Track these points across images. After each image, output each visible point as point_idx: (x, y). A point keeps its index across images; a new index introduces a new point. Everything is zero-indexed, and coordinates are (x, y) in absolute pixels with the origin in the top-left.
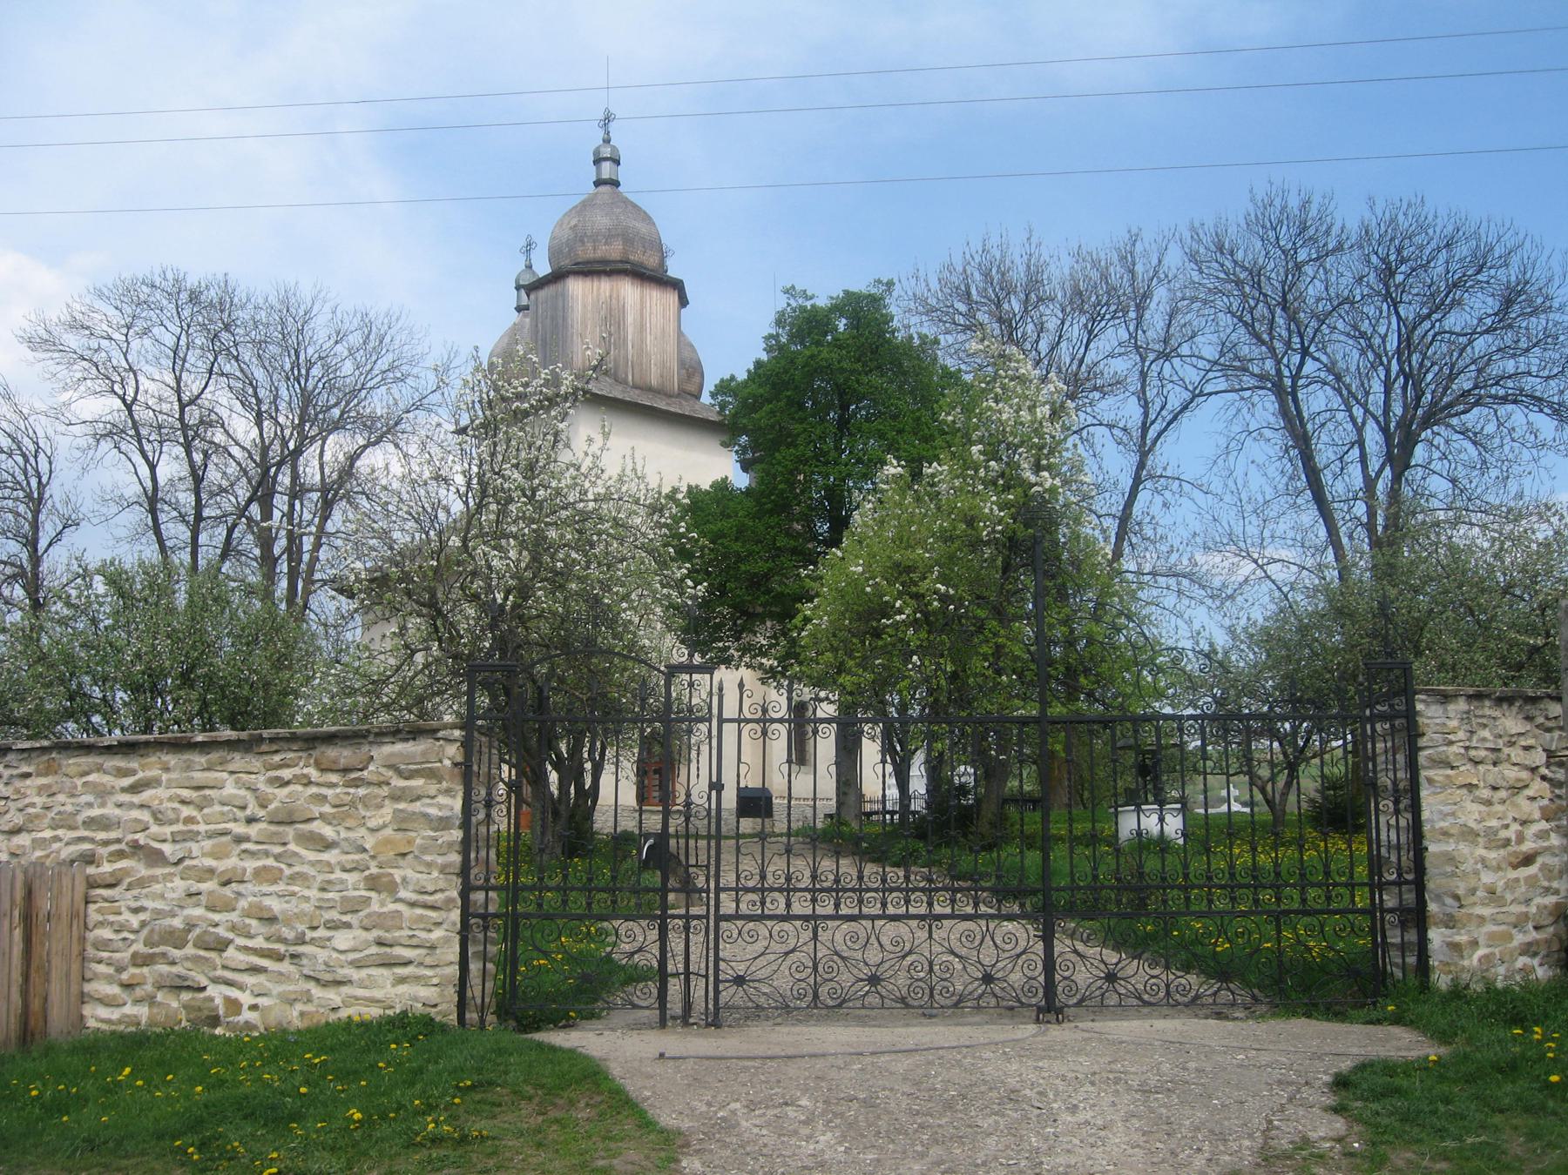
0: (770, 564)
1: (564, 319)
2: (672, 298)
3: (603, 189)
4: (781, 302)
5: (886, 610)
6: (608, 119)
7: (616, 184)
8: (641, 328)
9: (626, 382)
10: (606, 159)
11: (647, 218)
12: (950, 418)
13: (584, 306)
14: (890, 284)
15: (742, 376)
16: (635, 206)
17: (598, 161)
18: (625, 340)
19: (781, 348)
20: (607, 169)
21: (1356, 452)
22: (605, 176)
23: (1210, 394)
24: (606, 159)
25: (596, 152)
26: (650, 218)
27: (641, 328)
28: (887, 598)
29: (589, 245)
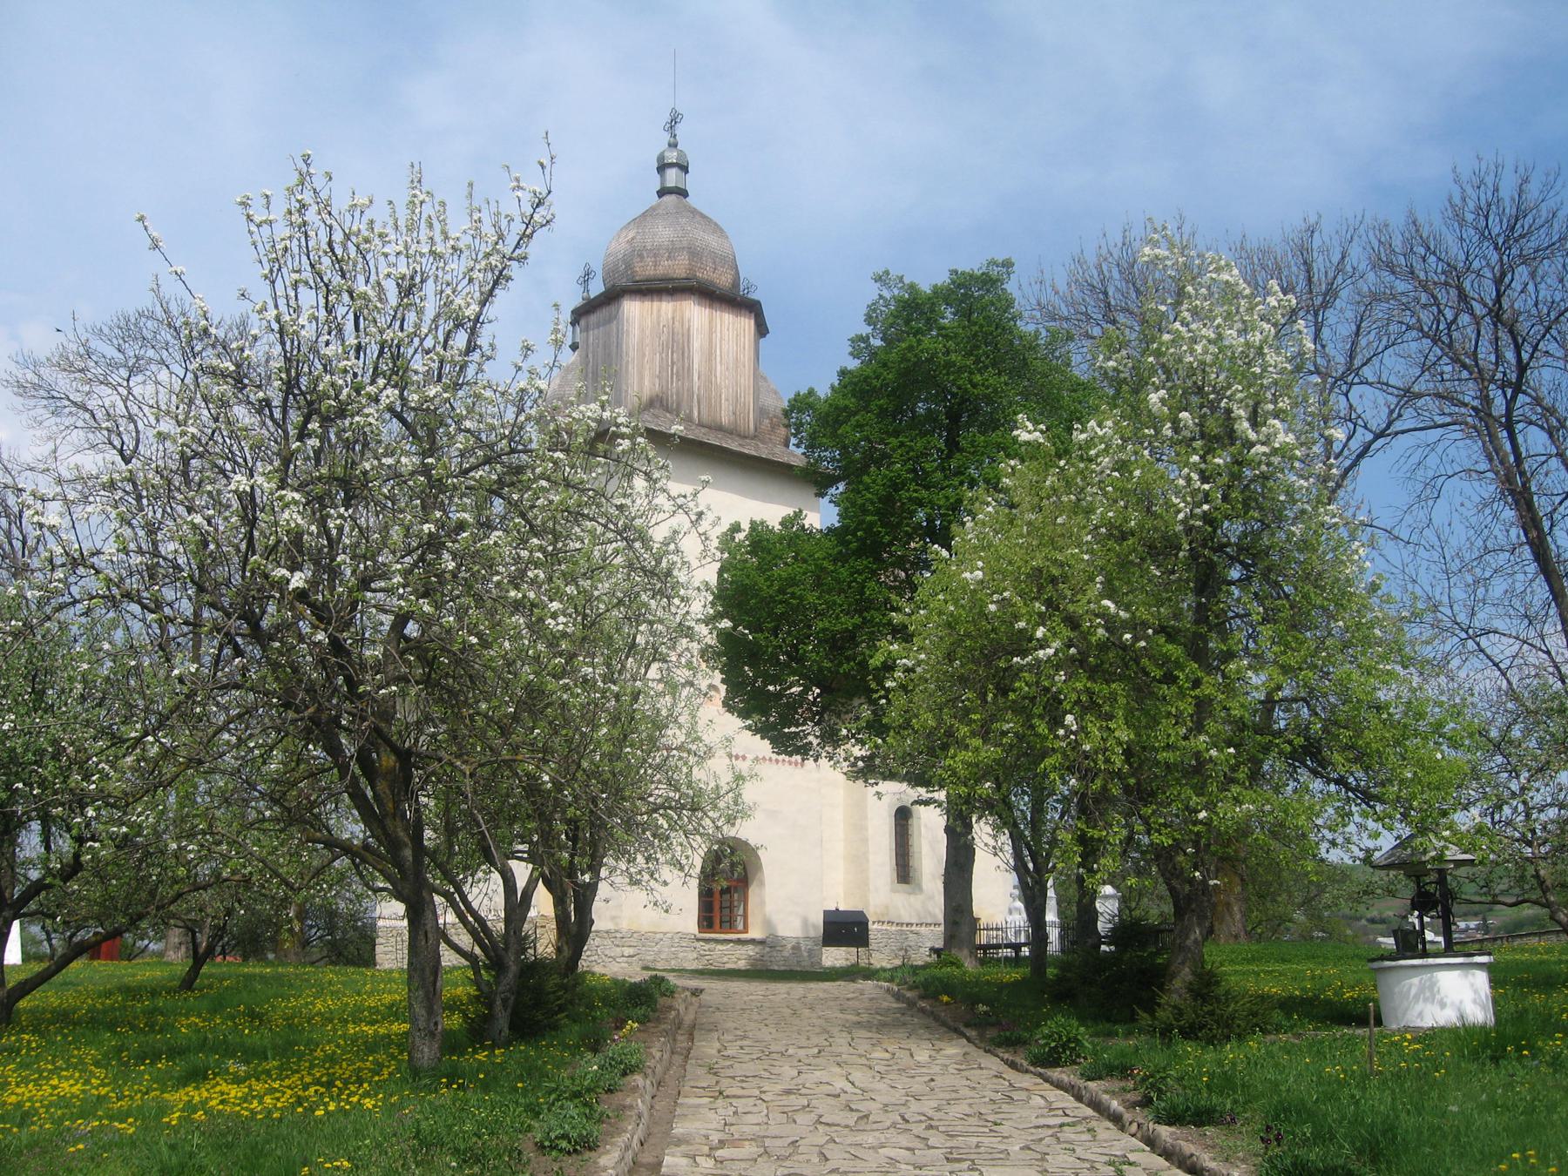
0: (857, 620)
1: (619, 345)
2: (747, 324)
3: (667, 198)
4: (872, 292)
5: (1023, 644)
6: (674, 121)
7: (683, 193)
8: (710, 356)
10: (671, 165)
11: (717, 229)
12: (1111, 363)
13: (642, 331)
14: (1008, 264)
15: (823, 391)
16: (703, 216)
17: (662, 167)
18: (690, 370)
19: (874, 354)
20: (672, 177)
22: (671, 183)
23: (1397, 433)
24: (671, 165)
25: (661, 158)
26: (722, 230)
27: (710, 356)
28: (1022, 624)
29: (649, 261)
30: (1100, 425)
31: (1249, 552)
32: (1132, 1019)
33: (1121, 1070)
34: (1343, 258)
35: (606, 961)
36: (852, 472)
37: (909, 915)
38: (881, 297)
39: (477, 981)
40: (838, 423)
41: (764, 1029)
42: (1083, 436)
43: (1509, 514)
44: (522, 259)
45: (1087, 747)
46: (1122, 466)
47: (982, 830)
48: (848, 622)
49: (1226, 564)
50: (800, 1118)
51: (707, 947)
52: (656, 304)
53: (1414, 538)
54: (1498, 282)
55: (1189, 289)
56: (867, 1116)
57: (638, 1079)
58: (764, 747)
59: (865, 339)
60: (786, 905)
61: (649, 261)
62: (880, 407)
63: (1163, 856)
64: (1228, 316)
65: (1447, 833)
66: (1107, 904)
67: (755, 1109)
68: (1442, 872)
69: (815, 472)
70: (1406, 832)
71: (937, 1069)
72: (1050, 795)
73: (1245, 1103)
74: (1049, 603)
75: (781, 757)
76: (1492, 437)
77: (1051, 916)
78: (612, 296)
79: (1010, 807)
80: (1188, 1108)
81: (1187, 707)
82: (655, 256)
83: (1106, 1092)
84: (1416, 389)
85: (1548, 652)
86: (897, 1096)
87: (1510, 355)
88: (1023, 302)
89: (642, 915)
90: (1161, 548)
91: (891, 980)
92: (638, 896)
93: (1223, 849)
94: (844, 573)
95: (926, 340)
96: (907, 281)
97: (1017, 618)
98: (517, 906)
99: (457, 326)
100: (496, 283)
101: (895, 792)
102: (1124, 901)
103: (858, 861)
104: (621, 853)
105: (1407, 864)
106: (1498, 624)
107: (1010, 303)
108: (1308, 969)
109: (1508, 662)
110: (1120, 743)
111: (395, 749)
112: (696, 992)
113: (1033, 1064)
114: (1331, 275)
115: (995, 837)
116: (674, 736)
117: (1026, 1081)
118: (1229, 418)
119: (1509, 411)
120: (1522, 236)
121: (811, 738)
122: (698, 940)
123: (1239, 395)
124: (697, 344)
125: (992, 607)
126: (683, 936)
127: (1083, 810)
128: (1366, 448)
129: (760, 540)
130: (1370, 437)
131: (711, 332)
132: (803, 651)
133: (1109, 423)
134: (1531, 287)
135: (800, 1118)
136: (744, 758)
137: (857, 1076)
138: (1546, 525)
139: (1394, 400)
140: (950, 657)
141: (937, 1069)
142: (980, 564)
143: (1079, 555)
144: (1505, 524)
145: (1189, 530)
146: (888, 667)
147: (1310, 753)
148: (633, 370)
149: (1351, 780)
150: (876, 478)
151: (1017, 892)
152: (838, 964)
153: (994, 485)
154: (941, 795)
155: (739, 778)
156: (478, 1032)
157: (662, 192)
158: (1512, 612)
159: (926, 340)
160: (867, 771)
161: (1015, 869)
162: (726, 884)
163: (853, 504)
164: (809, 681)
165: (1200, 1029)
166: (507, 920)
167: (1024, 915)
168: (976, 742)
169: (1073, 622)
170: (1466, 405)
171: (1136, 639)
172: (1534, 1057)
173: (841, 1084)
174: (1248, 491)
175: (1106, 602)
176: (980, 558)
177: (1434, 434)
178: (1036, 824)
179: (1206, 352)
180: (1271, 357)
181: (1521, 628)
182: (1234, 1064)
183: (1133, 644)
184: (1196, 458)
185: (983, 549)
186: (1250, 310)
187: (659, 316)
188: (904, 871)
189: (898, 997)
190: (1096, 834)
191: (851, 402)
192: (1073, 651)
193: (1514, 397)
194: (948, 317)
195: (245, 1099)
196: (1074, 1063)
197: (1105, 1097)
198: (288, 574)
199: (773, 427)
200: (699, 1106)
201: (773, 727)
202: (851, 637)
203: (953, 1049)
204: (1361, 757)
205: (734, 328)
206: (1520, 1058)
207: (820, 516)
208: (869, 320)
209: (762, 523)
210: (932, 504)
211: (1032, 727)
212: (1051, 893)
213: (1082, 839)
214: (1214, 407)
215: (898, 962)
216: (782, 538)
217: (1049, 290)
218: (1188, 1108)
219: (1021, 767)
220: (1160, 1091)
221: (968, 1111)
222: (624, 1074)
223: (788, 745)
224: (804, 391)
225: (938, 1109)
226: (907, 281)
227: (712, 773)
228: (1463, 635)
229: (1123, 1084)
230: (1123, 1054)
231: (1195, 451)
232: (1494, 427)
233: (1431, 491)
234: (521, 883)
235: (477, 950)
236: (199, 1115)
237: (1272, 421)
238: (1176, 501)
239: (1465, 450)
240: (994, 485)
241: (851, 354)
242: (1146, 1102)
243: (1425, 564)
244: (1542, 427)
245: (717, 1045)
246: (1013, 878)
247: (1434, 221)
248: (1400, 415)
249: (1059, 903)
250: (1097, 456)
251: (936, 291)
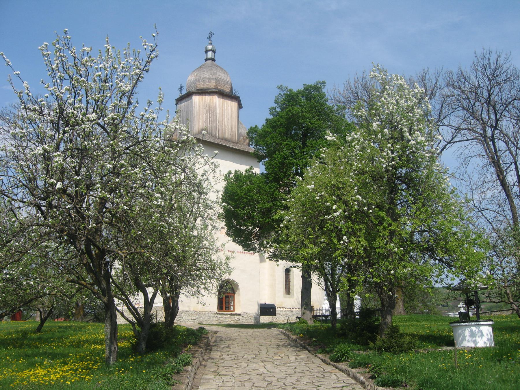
0: (271, 204)
2: (235, 104)
3: (207, 62)
4: (277, 92)
9: (216, 137)
10: (210, 50)
14: (324, 83)
15: (260, 127)
16: (220, 68)
18: (216, 119)
19: (278, 114)
20: (210, 54)
21: (513, 166)
23: (454, 142)
24: (210, 50)
28: (328, 204)
29: (202, 82)
30: (356, 134)
31: (409, 180)
32: (367, 344)
33: (362, 364)
34: (436, 82)
35: (184, 320)
36: (270, 154)
37: (289, 307)
38: (280, 94)
39: (134, 330)
40: (265, 137)
41: (237, 348)
42: (350, 138)
43: (493, 169)
44: (147, 71)
45: (351, 248)
46: (363, 149)
47: (314, 277)
48: (268, 205)
49: (402, 182)
50: (246, 384)
51: (221, 316)
52: (204, 97)
53: (461, 177)
54: (489, 91)
55: (387, 87)
56: (271, 383)
57: (189, 368)
58: (238, 248)
59: (275, 109)
60: (245, 305)
61: (202, 82)
62: (280, 131)
63: (378, 287)
64: (401, 96)
65: (478, 279)
66: (357, 303)
67: (230, 380)
68: (476, 292)
69: (257, 154)
70: (463, 277)
71: (297, 363)
72: (337, 265)
73: (410, 378)
74: (338, 196)
75: (246, 252)
76: (487, 144)
77: (338, 305)
78: (189, 95)
79: (324, 269)
80: (389, 380)
81: (387, 233)
82: (204, 81)
83: (358, 373)
84: (461, 127)
85: (505, 216)
86: (283, 375)
87: (493, 117)
88: (329, 97)
89: (196, 307)
90: (377, 178)
91: (283, 328)
92: (195, 300)
93: (395, 283)
94: (267, 188)
95: (295, 108)
96: (289, 88)
97: (326, 202)
98: (149, 304)
99: (123, 95)
100: (138, 79)
101: (284, 264)
102: (362, 301)
104: (187, 284)
105: (463, 289)
106: (489, 207)
107: (324, 95)
108: (425, 324)
109: (492, 220)
110: (362, 246)
111: (98, 248)
112: (216, 332)
113: (332, 361)
115: (319, 279)
116: (206, 243)
117: (329, 368)
118: (402, 132)
119: (493, 135)
120: (497, 76)
121: (256, 245)
123: (405, 123)
124: (218, 111)
125: (318, 198)
126: (212, 313)
127: (349, 269)
128: (445, 147)
129: (238, 176)
130: (446, 143)
132: (252, 216)
133: (359, 133)
134: (499, 93)
135: (246, 384)
137: (268, 366)
138: (505, 173)
139: (454, 131)
140: (303, 216)
141: (297, 363)
142: (313, 182)
143: (350, 179)
144: (491, 174)
145: (387, 170)
146: (281, 220)
147: (431, 250)
148: (196, 119)
149: (444, 260)
150: (278, 156)
151: (326, 297)
152: (265, 322)
153: (318, 157)
154: (300, 264)
155: (228, 259)
156: (135, 349)
157: (206, 60)
158: (493, 202)
159: (295, 108)
160: (275, 257)
161: (326, 290)
162: (226, 294)
163: (270, 165)
164: (255, 225)
165: (391, 348)
166: (145, 308)
167: (329, 305)
168: (312, 246)
169: (345, 203)
170: (477, 132)
171: (368, 209)
172: (513, 360)
173: (262, 370)
174: (409, 158)
175: (358, 196)
176: (314, 181)
177: (467, 142)
178: (332, 275)
179: (393, 108)
180: (416, 110)
181: (496, 208)
182: (405, 363)
183: (367, 212)
184: (389, 145)
185: (314, 177)
186: (409, 94)
187: (205, 101)
188: (288, 290)
189: (284, 334)
190: (354, 278)
191: (270, 130)
192: (346, 213)
193: (494, 130)
194: (303, 99)
195: (45, 375)
196: (346, 361)
197: (358, 375)
198: (55, 181)
199: (244, 140)
200: (210, 379)
201: (243, 241)
202: (269, 210)
203: (304, 355)
204: (446, 251)
205: (231, 106)
206: (508, 360)
207: (259, 169)
208: (276, 102)
209: (239, 171)
210: (297, 165)
211: (331, 241)
212: (338, 298)
213: (349, 280)
214: (396, 127)
215: (286, 321)
216: (245, 176)
217: (338, 93)
218: (389, 380)
219: (326, 254)
220: (378, 373)
221: (308, 381)
222: (184, 365)
223: (247, 246)
224: (253, 126)
225: (297, 381)
226: (289, 88)
227: (217, 257)
228: (477, 210)
229: (364, 370)
230: (364, 358)
231: (389, 143)
232: (487, 141)
233: (466, 162)
234: (150, 296)
235: (134, 320)
236: (25, 383)
237: (416, 132)
238: (383, 160)
239: (477, 148)
240: (318, 157)
241: (270, 114)
242: (373, 377)
243: (464, 186)
244: (503, 141)
245: (219, 354)
246: (325, 293)
247: (467, 69)
248: (456, 136)
249: (340, 301)
250: (355, 145)
251: (299, 92)
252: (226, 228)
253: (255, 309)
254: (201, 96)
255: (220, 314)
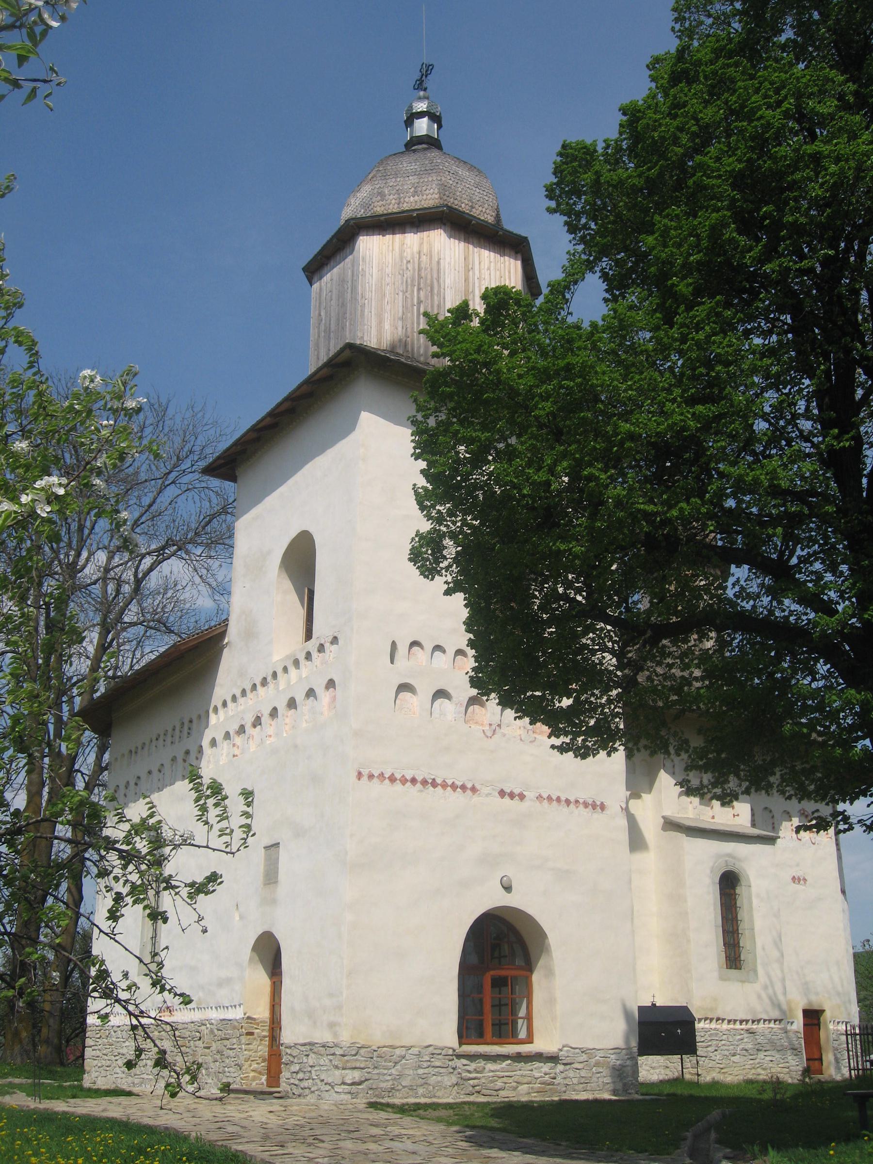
10: (421, 115)
13: (381, 270)
51: (473, 1066)
52: (398, 237)
103: (677, 939)
114: (209, 422)
122: (459, 1057)
126: (436, 1052)
131: (468, 269)
136: (522, 797)
187: (402, 252)
252: (471, 652)
253: (611, 1033)
254: (389, 237)
255: (472, 1057)
